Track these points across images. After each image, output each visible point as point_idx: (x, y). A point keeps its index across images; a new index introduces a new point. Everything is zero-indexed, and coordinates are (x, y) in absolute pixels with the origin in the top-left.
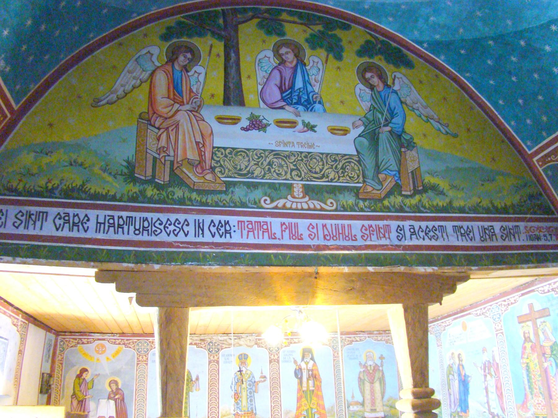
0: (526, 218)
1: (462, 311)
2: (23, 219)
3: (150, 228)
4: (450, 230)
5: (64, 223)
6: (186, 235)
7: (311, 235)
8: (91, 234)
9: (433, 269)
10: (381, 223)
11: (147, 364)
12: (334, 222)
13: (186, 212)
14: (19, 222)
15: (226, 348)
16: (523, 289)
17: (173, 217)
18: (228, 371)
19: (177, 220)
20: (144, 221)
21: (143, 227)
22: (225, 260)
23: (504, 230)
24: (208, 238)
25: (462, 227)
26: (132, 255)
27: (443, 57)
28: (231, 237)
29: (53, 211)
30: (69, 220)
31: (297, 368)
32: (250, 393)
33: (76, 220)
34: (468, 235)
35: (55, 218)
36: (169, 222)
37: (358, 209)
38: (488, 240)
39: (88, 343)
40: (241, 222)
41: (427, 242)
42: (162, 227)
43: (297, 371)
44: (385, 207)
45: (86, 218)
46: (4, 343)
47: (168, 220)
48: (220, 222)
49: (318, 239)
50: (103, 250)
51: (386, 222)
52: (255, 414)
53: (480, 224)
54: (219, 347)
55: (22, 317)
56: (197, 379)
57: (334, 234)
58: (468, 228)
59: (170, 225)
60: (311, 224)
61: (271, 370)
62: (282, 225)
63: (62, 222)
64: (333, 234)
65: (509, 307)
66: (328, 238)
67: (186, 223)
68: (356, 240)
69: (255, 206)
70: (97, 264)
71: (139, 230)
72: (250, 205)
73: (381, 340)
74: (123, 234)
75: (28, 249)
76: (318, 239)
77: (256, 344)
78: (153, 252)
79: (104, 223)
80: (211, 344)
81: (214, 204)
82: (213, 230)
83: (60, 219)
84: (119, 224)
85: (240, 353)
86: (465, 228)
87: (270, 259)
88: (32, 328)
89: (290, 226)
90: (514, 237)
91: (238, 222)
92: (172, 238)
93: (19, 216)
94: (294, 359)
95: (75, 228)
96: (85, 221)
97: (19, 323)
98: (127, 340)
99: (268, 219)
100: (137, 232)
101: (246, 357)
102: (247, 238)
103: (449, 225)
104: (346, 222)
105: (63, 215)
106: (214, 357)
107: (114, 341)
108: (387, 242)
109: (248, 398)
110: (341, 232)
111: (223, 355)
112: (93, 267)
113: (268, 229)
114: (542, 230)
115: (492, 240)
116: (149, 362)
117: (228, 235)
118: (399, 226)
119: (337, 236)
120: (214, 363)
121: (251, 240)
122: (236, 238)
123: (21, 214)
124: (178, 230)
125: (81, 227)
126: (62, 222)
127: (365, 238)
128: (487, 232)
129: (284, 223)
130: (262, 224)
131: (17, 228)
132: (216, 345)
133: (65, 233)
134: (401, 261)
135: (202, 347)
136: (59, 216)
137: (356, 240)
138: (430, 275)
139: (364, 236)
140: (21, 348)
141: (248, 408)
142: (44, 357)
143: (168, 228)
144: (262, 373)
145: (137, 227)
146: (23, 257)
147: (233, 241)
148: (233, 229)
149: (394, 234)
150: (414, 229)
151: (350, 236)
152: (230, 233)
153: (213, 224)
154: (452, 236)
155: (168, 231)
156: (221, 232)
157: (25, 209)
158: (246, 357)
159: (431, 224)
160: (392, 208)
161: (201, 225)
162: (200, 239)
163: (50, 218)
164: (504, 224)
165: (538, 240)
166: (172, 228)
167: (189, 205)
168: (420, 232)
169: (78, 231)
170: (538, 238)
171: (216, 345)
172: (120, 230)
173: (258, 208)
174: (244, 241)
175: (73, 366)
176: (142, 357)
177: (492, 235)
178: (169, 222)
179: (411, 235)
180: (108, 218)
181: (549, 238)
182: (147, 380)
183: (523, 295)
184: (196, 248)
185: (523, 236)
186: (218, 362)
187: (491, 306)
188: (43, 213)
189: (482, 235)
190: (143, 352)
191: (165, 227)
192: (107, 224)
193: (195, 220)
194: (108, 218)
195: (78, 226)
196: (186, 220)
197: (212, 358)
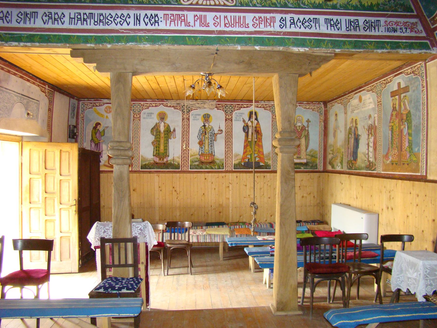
0: (387, 14)
1: (360, 88)
2: (22, 17)
3: (104, 21)
4: (322, 21)
5: (49, 19)
6: (128, 25)
7: (216, 23)
8: (66, 26)
9: (305, 50)
10: (268, 16)
11: (140, 120)
12: (233, 14)
13: (128, 8)
14: (20, 19)
16: (396, 72)
17: (119, 12)
18: (196, 125)
19: (122, 14)
20: (100, 16)
21: (100, 20)
22: (153, 40)
23: (367, 23)
24: (143, 26)
25: (332, 19)
26: (93, 39)
28: (158, 25)
29: (41, 12)
30: (52, 17)
31: (245, 125)
32: (211, 141)
33: (56, 17)
34: (336, 26)
35: (43, 16)
36: (117, 16)
37: (252, 5)
38: (353, 30)
39: (100, 106)
40: (166, 15)
41: (303, 30)
42: (112, 20)
43: (245, 128)
44: (272, 4)
45: (63, 15)
46: (37, 103)
47: (116, 14)
48: (151, 15)
49: (220, 27)
50: (75, 36)
51: (272, 15)
52: (214, 155)
53: (348, 18)
55: (49, 87)
56: (174, 130)
57: (233, 23)
58: (337, 20)
59: (117, 18)
60: (216, 16)
61: (226, 126)
62: (195, 17)
63: (47, 18)
65: (387, 85)
66: (228, 26)
67: (128, 16)
68: (248, 27)
69: (177, 4)
70: (71, 45)
71: (97, 22)
72: (173, 3)
73: (309, 108)
74: (87, 25)
75: (27, 37)
76: (220, 27)
77: (216, 107)
78: (107, 36)
79: (74, 18)
81: (147, 3)
82: (147, 20)
83: (46, 16)
84: (84, 19)
85: (205, 113)
86: (335, 21)
87: (186, 40)
88: (57, 96)
89: (200, 18)
90: (375, 29)
91: (164, 14)
92: (119, 27)
93: (20, 15)
94: (243, 119)
95: (56, 22)
96: (62, 17)
97: (47, 91)
99: (185, 13)
100: (96, 23)
102: (170, 26)
103: (322, 18)
104: (242, 15)
105: (48, 14)
108: (272, 29)
109: (209, 145)
110: (237, 21)
112: (69, 47)
113: (184, 19)
114: (399, 24)
115: (355, 30)
116: (142, 119)
117: (157, 24)
118: (282, 18)
119: (235, 24)
120: (186, 121)
121: (173, 27)
122: (162, 26)
123: (21, 14)
124: (123, 21)
125: (59, 21)
126: (47, 18)
127: (255, 26)
128: (353, 24)
129: (196, 15)
130: (181, 16)
131: (19, 23)
133: (50, 25)
134: (281, 42)
135: (177, 109)
136: (45, 15)
137: (248, 27)
138: (304, 55)
139: (255, 25)
140: (50, 108)
142: (70, 115)
143: (116, 20)
144: (220, 128)
145: (96, 20)
146: (24, 42)
147: (160, 28)
148: (160, 19)
149: (277, 23)
150: (294, 20)
151: (244, 25)
152: (158, 23)
153: (146, 17)
154: (323, 26)
155: (116, 22)
156: (152, 22)
157: (23, 10)
158: (208, 116)
159: (307, 17)
160: (278, 5)
161: (138, 17)
162: (138, 27)
163: (40, 16)
164: (368, 19)
165: (394, 32)
166: (119, 20)
167: (131, 4)
168: (298, 23)
169: (58, 24)
170: (395, 31)
172: (85, 22)
173: (178, 4)
174: (168, 28)
175: (91, 121)
176: (137, 115)
177: (356, 27)
178: (117, 16)
179: (291, 24)
180: (76, 15)
181: (404, 30)
183: (396, 76)
184: (135, 33)
185: (382, 29)
187: (376, 84)
188: (35, 12)
189: (347, 26)
191: (114, 20)
192: (76, 19)
193: (135, 14)
194: (76, 15)
195: (58, 21)
196: (128, 14)
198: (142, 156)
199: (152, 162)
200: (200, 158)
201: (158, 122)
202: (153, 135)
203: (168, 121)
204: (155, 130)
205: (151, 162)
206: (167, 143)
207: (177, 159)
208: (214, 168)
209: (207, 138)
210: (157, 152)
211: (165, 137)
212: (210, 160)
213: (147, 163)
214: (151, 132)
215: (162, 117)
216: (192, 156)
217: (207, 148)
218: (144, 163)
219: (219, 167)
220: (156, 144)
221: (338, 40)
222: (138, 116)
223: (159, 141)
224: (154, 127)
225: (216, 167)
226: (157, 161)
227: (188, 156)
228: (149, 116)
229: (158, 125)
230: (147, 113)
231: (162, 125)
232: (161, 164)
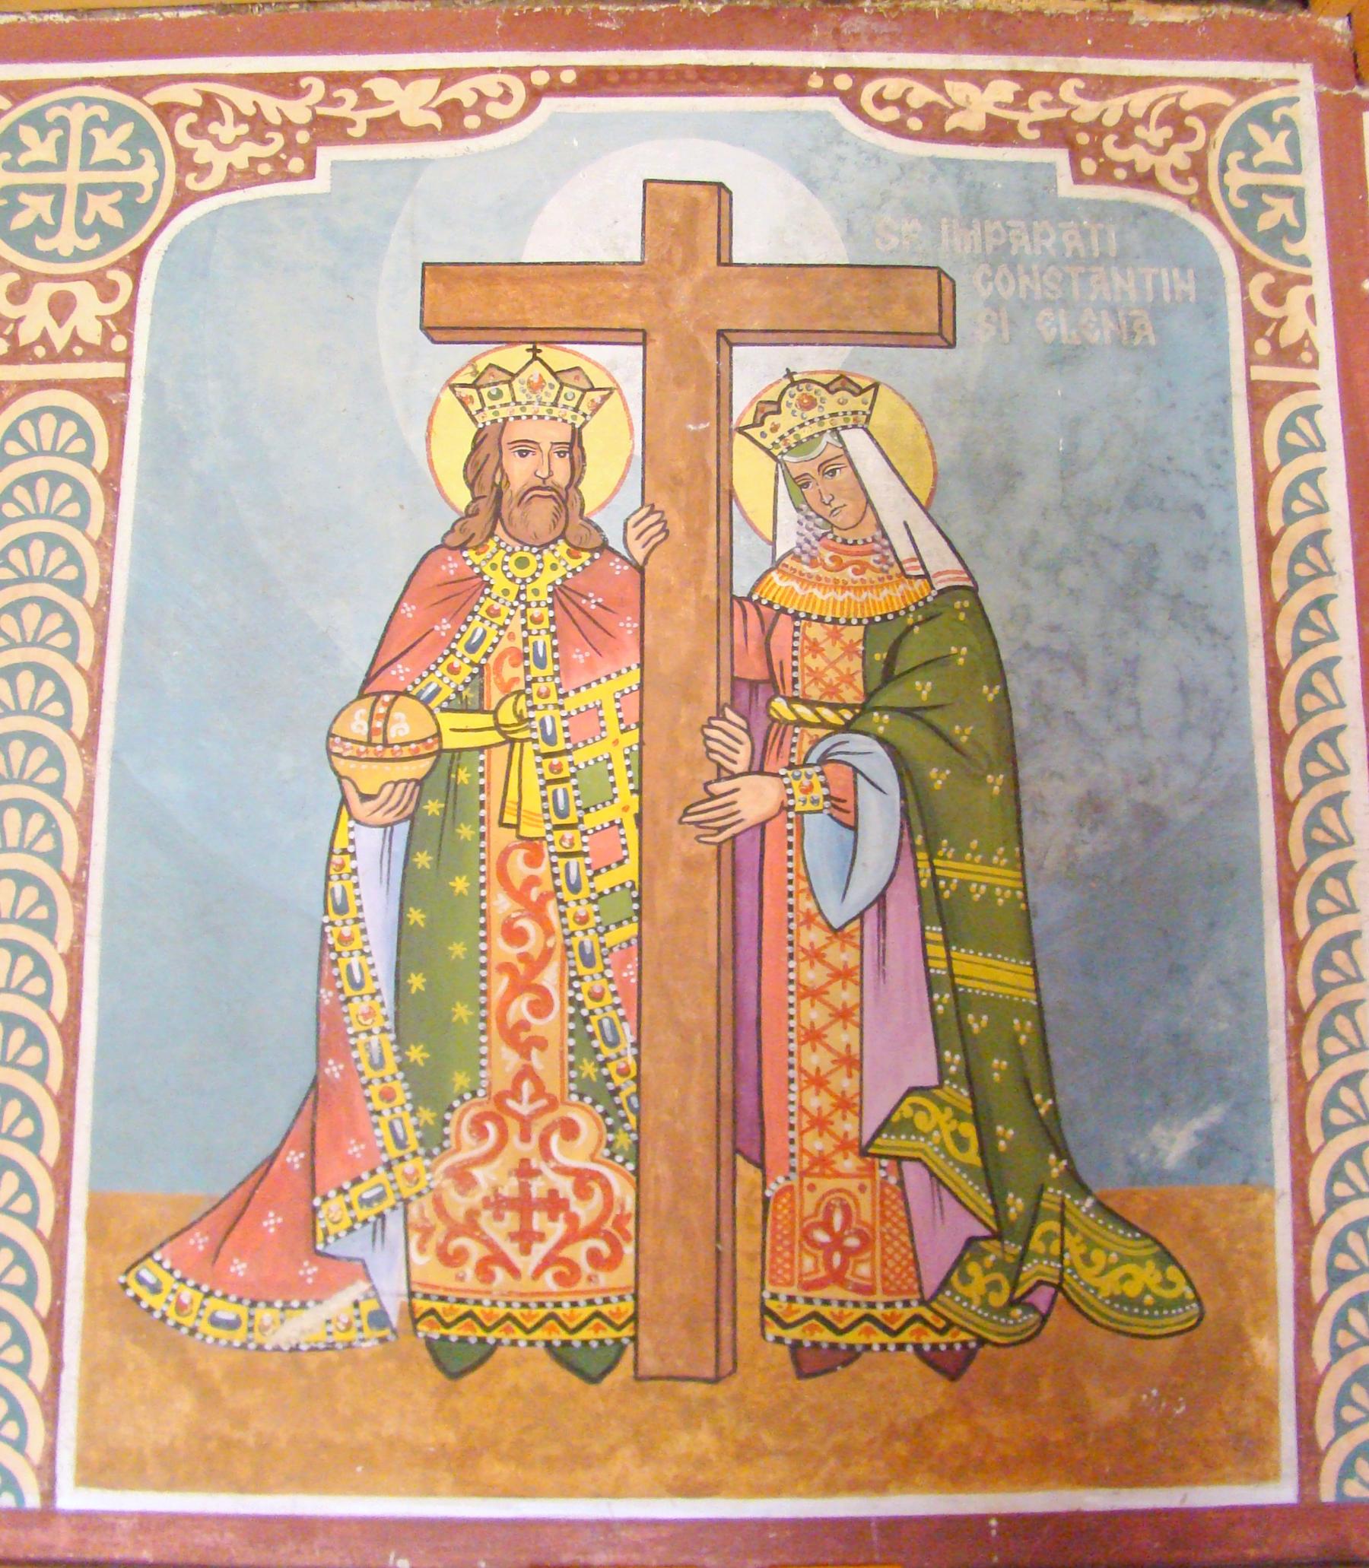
27: (271, 1214)
98: (1100, 87)
107: (921, 95)
190: (66, 240)
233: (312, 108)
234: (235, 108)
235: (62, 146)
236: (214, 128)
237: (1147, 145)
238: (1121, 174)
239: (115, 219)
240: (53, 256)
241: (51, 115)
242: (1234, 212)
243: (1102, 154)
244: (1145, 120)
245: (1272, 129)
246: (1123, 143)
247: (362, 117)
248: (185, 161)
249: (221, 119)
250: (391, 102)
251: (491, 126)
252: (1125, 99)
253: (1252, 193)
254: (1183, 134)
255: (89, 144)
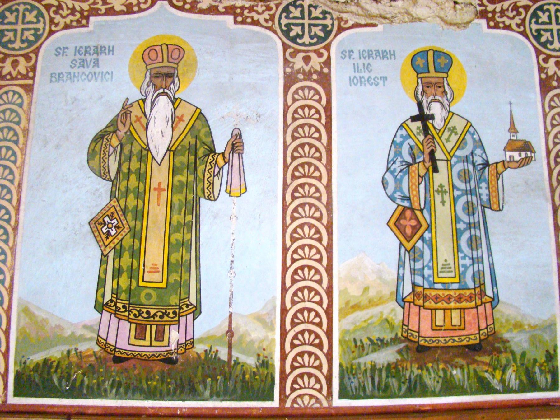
11: (29, 89)
15: (357, 25)
18: (368, 118)
32: (470, 209)
52: (494, 301)
54: (328, 22)
56: (236, 144)
64: (217, 389)
77: (483, 14)
80: (296, 13)
101: (442, 61)
106: (307, 59)
109: (458, 234)
111: (346, 54)
116: (41, 82)
132: (316, 13)
135: (256, 23)
141: (461, 276)
144: (513, 129)
158: (442, 61)
171: (316, 13)
182: (23, 152)
186: (325, 80)
190: (18, 45)
197: (298, 63)
198: (26, 311)
199: (89, 347)
200: (405, 324)
201: (135, 95)
202: (102, 172)
203: (196, 90)
204: (116, 146)
205: (83, 347)
206: (186, 226)
207: (256, 333)
208: (495, 383)
209: (441, 191)
210: (124, 282)
211: (176, 189)
212: (471, 335)
213: (55, 353)
214: (91, 154)
215: (164, 69)
216: (352, 307)
217: (445, 252)
218: (37, 358)
219: (529, 374)
220: (116, 231)
221: (150, 395)
222: (23, 66)
223: (138, 214)
224: (112, 128)
225: (511, 376)
226: (122, 344)
227: (329, 312)
228: (83, 63)
229: (136, 112)
230: (78, 51)
231: (163, 108)
232: (146, 360)
233: (89, 5)
234: (67, 6)
235: (17, 18)
236: (61, 12)
237: (508, 17)
238: (501, 25)
239: (32, 38)
240: (14, 49)
241: (14, 8)
242: (282, 30)
243: (495, 19)
244: (508, 10)
245: (544, 12)
246: (501, 17)
247: (103, 8)
248: (52, 20)
249: (63, 9)
250: (111, 4)
251: (141, 10)
252: (502, 4)
253: (538, 31)
254: (519, 14)
255: (24, 16)
